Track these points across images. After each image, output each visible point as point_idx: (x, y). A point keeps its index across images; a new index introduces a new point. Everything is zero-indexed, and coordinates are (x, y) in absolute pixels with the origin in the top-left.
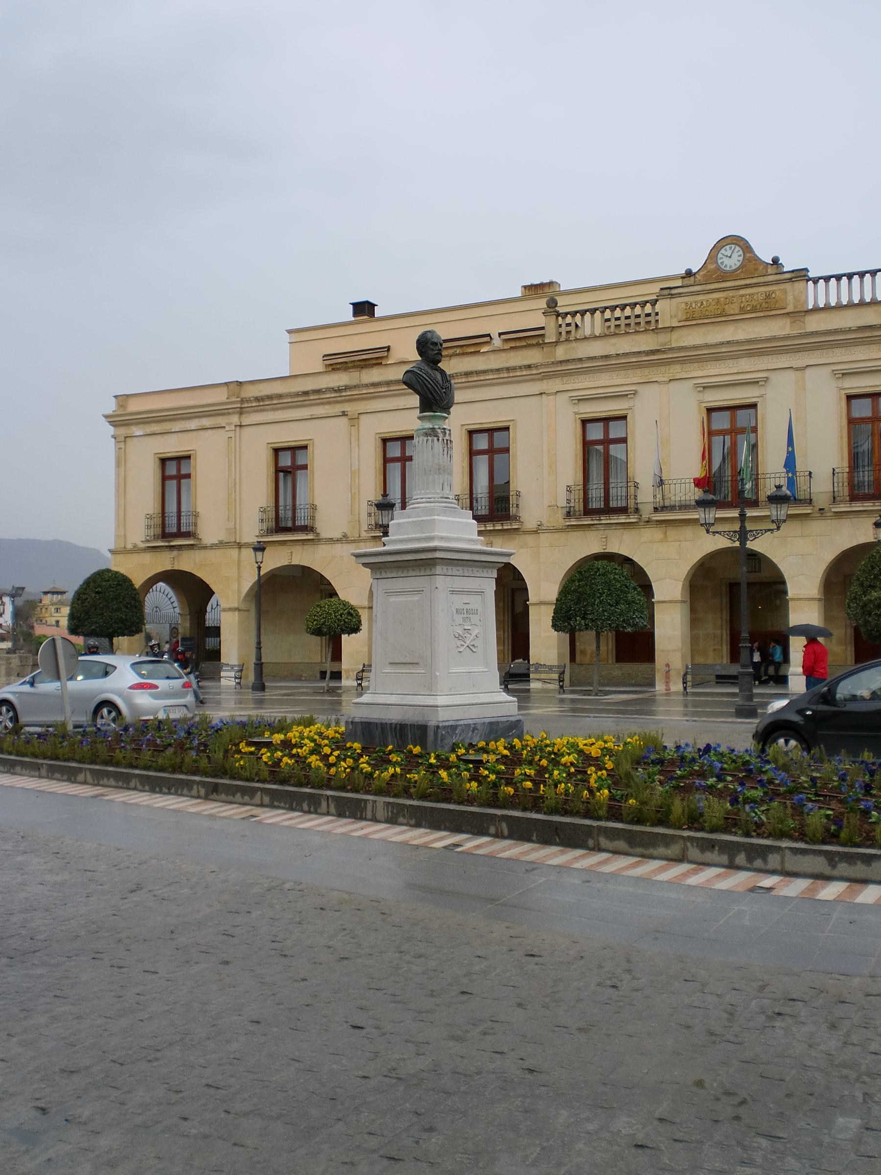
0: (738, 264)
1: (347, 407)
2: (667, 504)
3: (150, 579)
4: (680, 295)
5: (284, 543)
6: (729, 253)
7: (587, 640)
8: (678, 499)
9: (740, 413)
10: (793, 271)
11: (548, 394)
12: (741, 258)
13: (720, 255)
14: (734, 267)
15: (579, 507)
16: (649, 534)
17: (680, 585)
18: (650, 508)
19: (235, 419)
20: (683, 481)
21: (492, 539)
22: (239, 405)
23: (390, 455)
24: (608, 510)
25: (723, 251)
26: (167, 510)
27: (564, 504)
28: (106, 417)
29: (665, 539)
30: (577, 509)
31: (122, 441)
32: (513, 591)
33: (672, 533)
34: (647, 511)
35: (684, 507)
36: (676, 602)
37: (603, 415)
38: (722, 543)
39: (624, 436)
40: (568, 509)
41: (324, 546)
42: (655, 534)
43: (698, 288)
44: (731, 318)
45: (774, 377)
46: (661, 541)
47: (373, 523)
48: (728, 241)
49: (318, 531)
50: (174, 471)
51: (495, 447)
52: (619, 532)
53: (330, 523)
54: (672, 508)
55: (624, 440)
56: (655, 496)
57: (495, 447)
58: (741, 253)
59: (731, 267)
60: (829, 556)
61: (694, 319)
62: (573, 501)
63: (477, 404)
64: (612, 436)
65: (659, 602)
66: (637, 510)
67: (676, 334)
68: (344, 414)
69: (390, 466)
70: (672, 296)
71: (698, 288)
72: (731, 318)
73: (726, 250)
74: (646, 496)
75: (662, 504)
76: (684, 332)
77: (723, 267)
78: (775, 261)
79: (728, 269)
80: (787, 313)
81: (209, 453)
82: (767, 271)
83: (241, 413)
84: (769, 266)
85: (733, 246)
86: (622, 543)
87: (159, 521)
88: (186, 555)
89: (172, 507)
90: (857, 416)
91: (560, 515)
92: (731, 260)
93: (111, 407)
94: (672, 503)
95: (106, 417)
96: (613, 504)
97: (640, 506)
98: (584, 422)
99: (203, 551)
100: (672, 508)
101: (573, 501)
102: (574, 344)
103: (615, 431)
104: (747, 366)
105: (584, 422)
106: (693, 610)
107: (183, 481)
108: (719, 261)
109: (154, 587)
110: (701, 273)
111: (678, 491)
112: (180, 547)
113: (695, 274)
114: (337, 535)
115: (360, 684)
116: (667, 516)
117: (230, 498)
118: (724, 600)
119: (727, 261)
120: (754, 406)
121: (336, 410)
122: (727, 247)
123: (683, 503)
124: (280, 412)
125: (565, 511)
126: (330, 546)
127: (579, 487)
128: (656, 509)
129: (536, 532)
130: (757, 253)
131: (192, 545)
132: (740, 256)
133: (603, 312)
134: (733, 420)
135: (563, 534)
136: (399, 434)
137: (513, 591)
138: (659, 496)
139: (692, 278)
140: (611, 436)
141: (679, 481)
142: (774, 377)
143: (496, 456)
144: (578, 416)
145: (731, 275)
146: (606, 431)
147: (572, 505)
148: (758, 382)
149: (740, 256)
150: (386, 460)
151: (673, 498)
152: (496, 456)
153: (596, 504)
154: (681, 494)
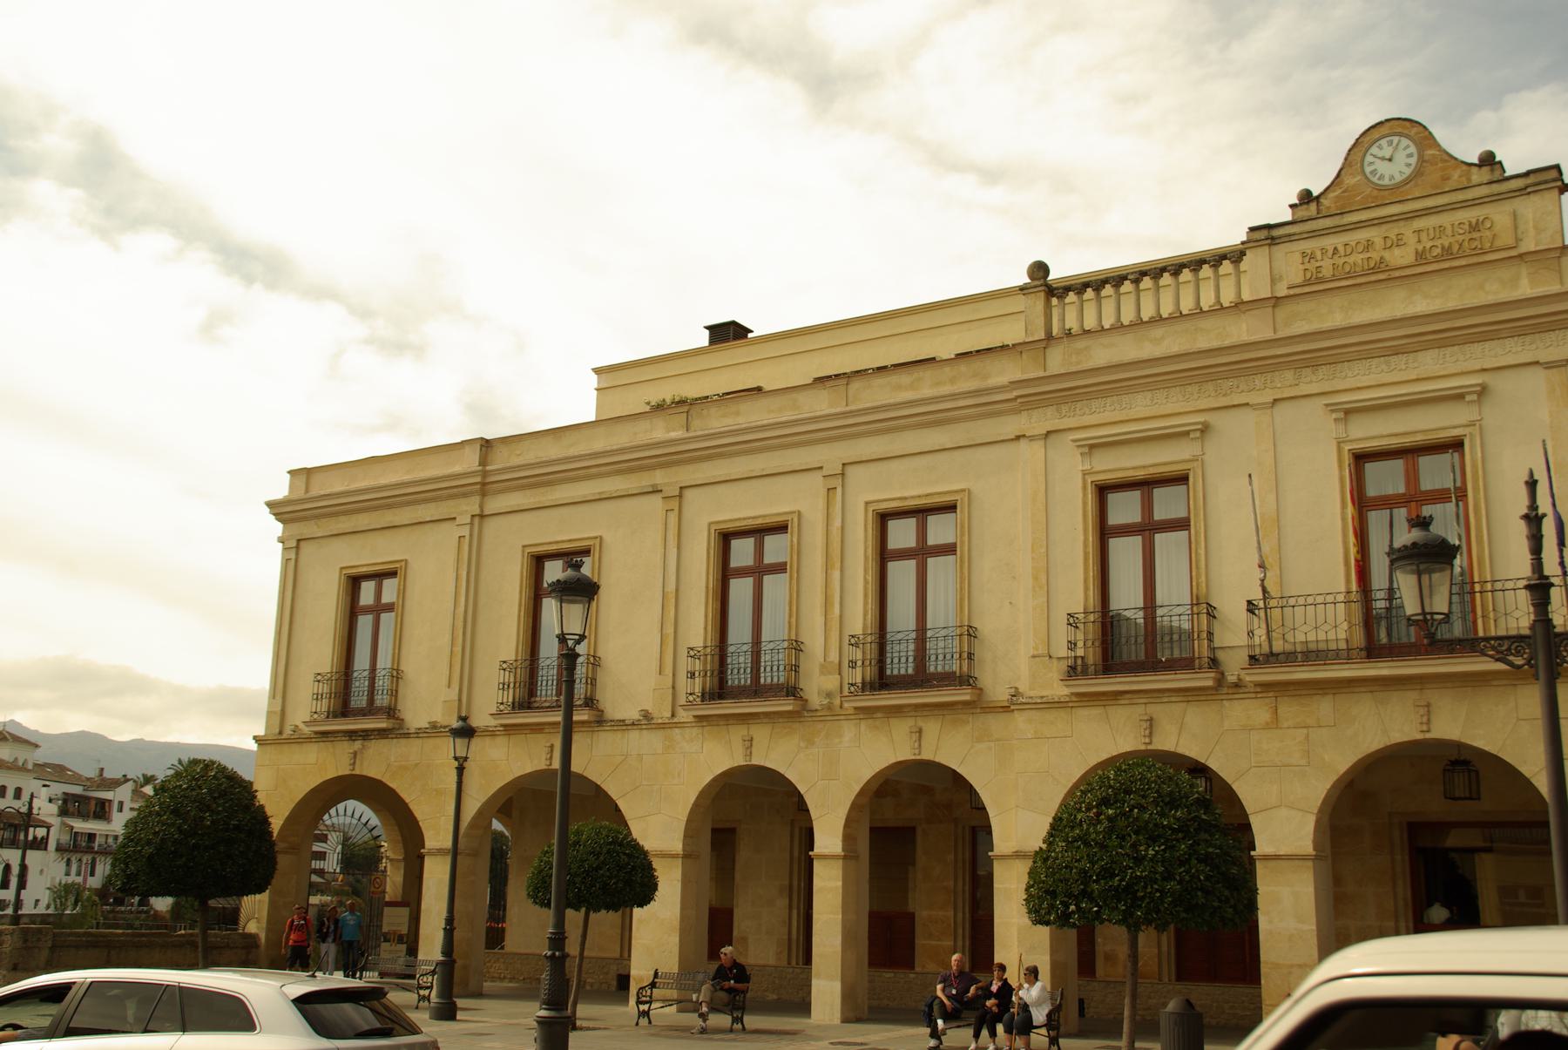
0: (1408, 171)
1: (659, 477)
2: (1278, 646)
3: (314, 792)
4: (1290, 238)
5: (897, 711)
6: (1387, 152)
7: (1112, 938)
8: (1301, 637)
9: (1424, 461)
10: (1528, 174)
11: (1032, 438)
12: (1413, 160)
13: (1369, 158)
14: (1398, 178)
15: (1093, 656)
16: (1247, 712)
17: (1309, 825)
18: (1242, 657)
19: (471, 506)
20: (1310, 600)
21: (921, 723)
22: (478, 479)
23: (1114, 519)
24: (921, 679)
25: (1374, 150)
26: (891, 626)
27: (1063, 652)
28: (270, 505)
29: (1275, 723)
30: (1090, 661)
31: (294, 549)
32: (974, 830)
33: (1290, 709)
34: (1235, 665)
35: (1312, 655)
36: (1303, 858)
37: (1140, 474)
38: (539, 763)
39: (1183, 514)
40: (1070, 662)
41: (609, 734)
42: (1254, 711)
43: (1328, 222)
44: (1397, 274)
45: (1502, 384)
46: (1267, 727)
47: (859, 680)
48: (1384, 130)
49: (601, 707)
50: (363, 599)
51: (1157, 517)
52: (1177, 709)
53: (426, 701)
54: (1289, 658)
55: (1182, 524)
56: (1251, 633)
57: (1157, 517)
58: (1413, 149)
59: (1392, 178)
60: (1341, 761)
61: (1321, 281)
62: (1080, 644)
63: (894, 464)
64: (1159, 514)
65: (1267, 858)
66: (1214, 663)
67: (1283, 312)
68: (656, 491)
69: (1114, 543)
70: (1273, 241)
71: (1328, 222)
72: (1397, 274)
73: (1380, 148)
74: (1236, 634)
75: (1266, 649)
76: (1302, 306)
77: (1375, 180)
78: (1488, 160)
79: (1386, 182)
80: (1521, 256)
81: (430, 565)
82: (1469, 180)
83: (484, 494)
84: (1475, 170)
85: (1396, 139)
86: (1188, 732)
87: (871, 651)
88: (376, 747)
89: (740, 632)
90: (1429, 487)
91: (1056, 671)
92: (1392, 163)
93: (281, 489)
94: (1289, 648)
95: (270, 505)
96: (765, 678)
97: (1220, 655)
98: (1361, 458)
99: (403, 741)
100: (1289, 658)
101: (1080, 644)
102: (1080, 344)
103: (1167, 504)
104: (1174, 406)
105: (1103, 491)
106: (1337, 880)
107: (383, 616)
108: (1368, 170)
109: (341, 806)
110: (1331, 195)
111: (1321, 620)
112: (366, 735)
113: (1318, 197)
114: (633, 714)
115: (646, 1014)
116: (1286, 674)
117: (455, 643)
118: (1398, 858)
119: (1383, 168)
120: (1457, 445)
121: (644, 483)
122: (1383, 142)
123: (1312, 647)
124: (342, 518)
125: (1064, 665)
126: (619, 735)
127: (745, 648)
128: (1253, 659)
129: (1006, 709)
130: (1444, 145)
131: (384, 730)
132: (1410, 156)
133: (1137, 282)
134: (1412, 476)
135: (1062, 713)
136: (751, 522)
137: (974, 830)
138: (1260, 633)
139: (1313, 206)
140: (931, 541)
141: (1301, 601)
142: (1502, 384)
143: (766, 578)
144: (713, 528)
145: (1395, 192)
146: (1148, 506)
147: (1080, 652)
148: (1188, 433)
149: (1410, 156)
150: (1105, 532)
151: (1289, 637)
152: (766, 578)
153: (901, 662)
154: (1327, 627)
